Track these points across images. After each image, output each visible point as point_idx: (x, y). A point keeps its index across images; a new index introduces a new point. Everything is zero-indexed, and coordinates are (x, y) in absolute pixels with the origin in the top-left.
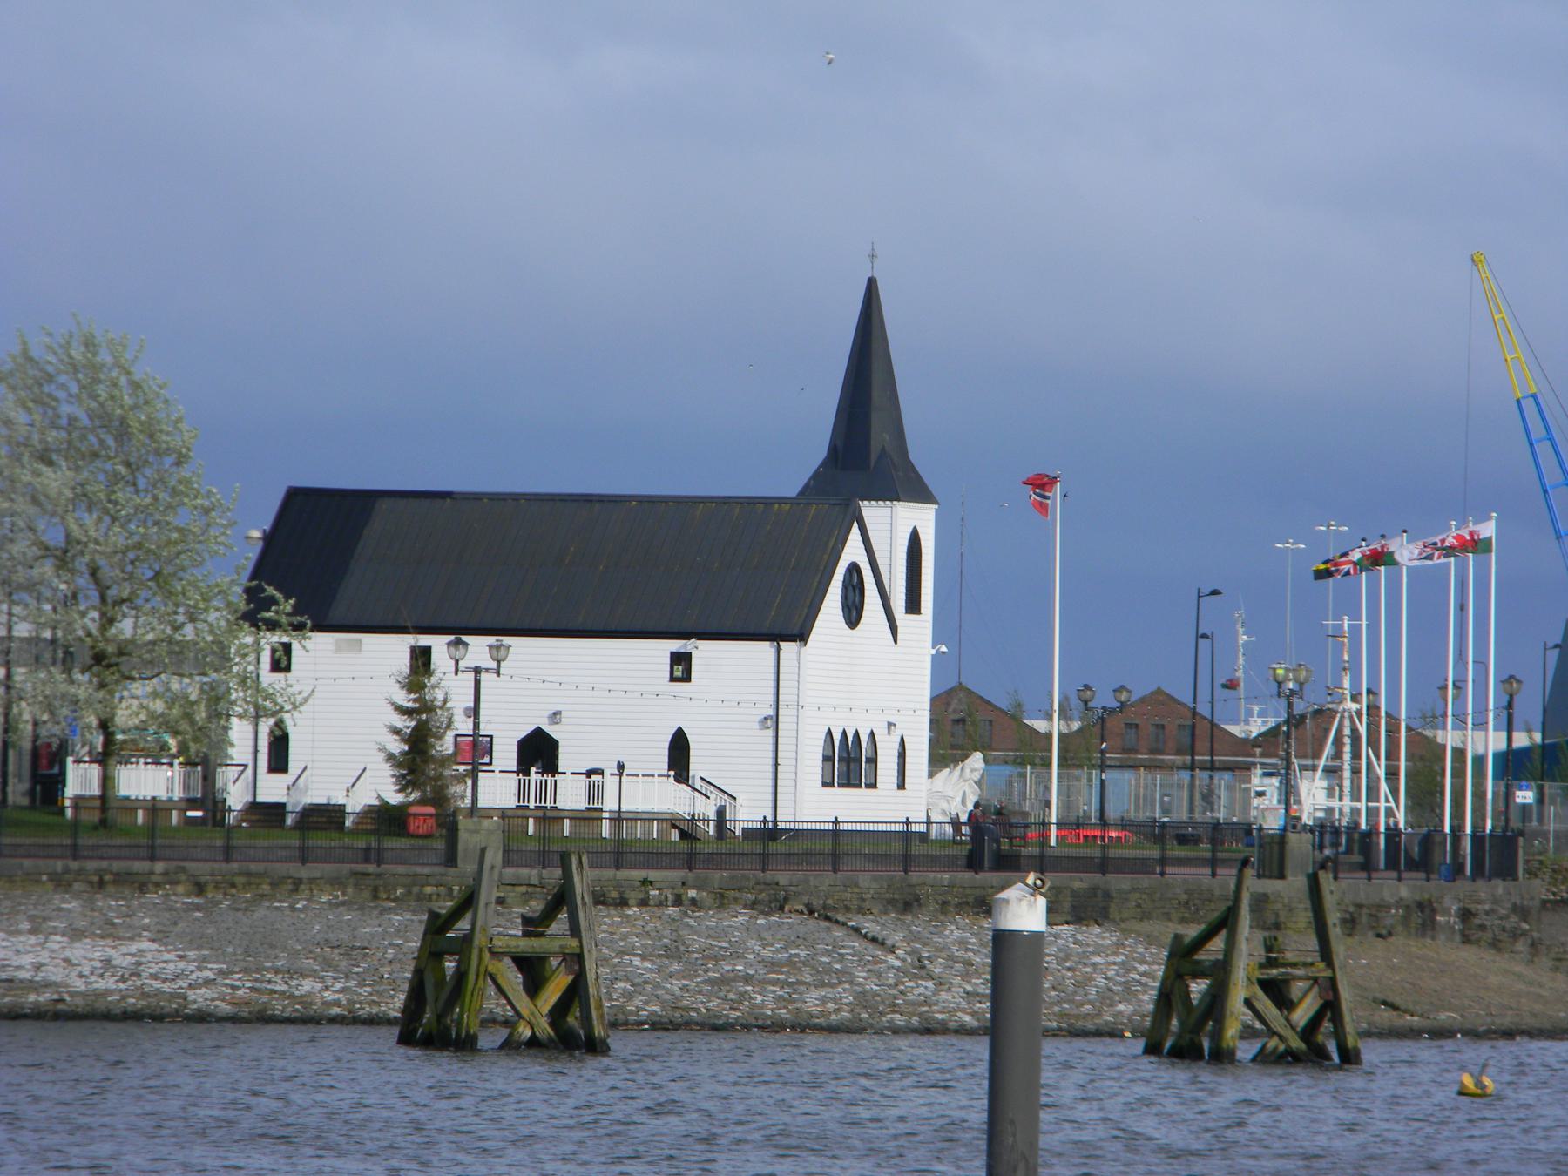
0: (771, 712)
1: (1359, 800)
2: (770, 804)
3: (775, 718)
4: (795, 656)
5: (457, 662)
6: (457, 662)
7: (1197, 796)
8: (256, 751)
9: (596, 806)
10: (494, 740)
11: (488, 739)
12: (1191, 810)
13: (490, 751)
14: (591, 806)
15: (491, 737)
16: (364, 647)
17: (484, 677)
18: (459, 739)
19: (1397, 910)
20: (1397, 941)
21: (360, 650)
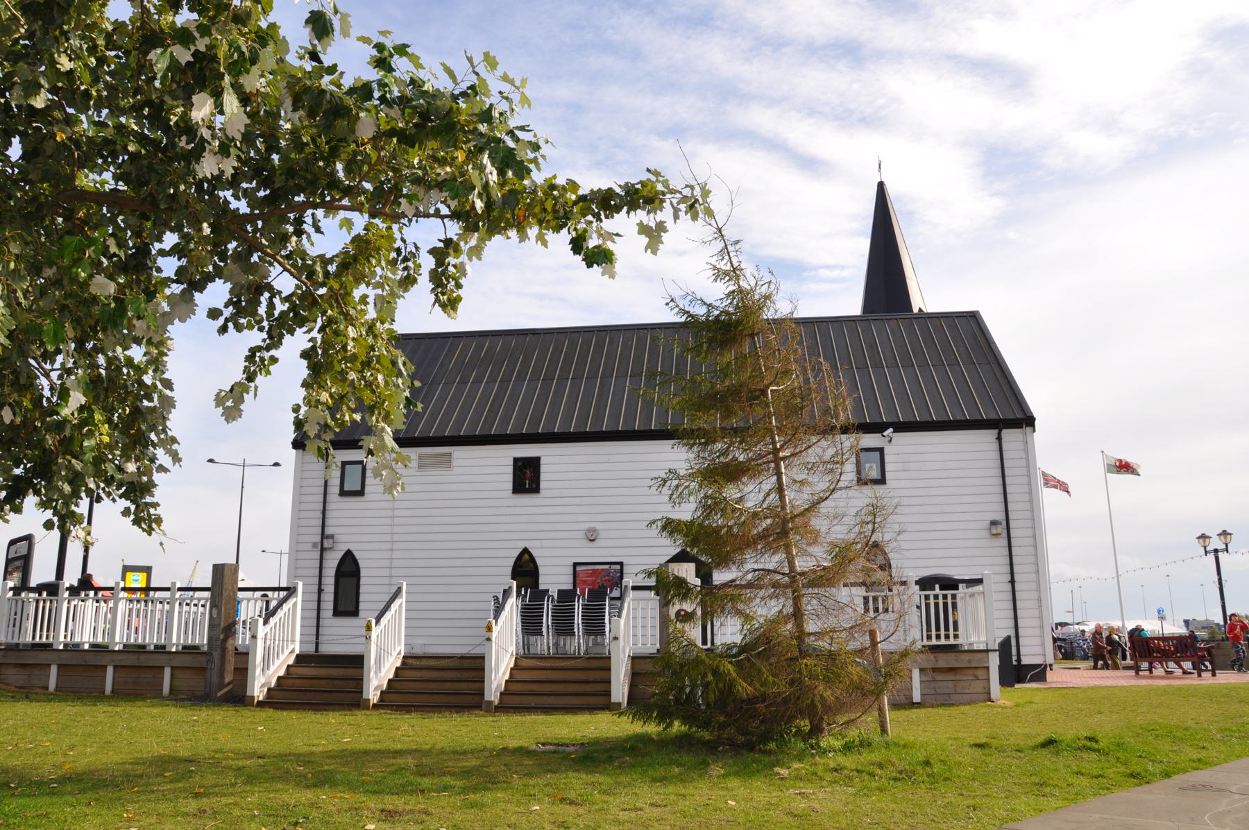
0: (1000, 516)
1: (948, 630)
2: (1011, 623)
3: (1004, 523)
4: (1020, 446)
5: (1205, 547)
6: (1205, 547)
7: (576, 634)
8: (320, 591)
9: (943, 641)
10: (626, 570)
11: (618, 567)
12: (34, 637)
13: (9, 562)
14: (934, 642)
15: (621, 564)
16: (455, 463)
17: (1220, 554)
18: (579, 568)
19: (287, 221)
20: (579, 258)
21: (450, 467)
